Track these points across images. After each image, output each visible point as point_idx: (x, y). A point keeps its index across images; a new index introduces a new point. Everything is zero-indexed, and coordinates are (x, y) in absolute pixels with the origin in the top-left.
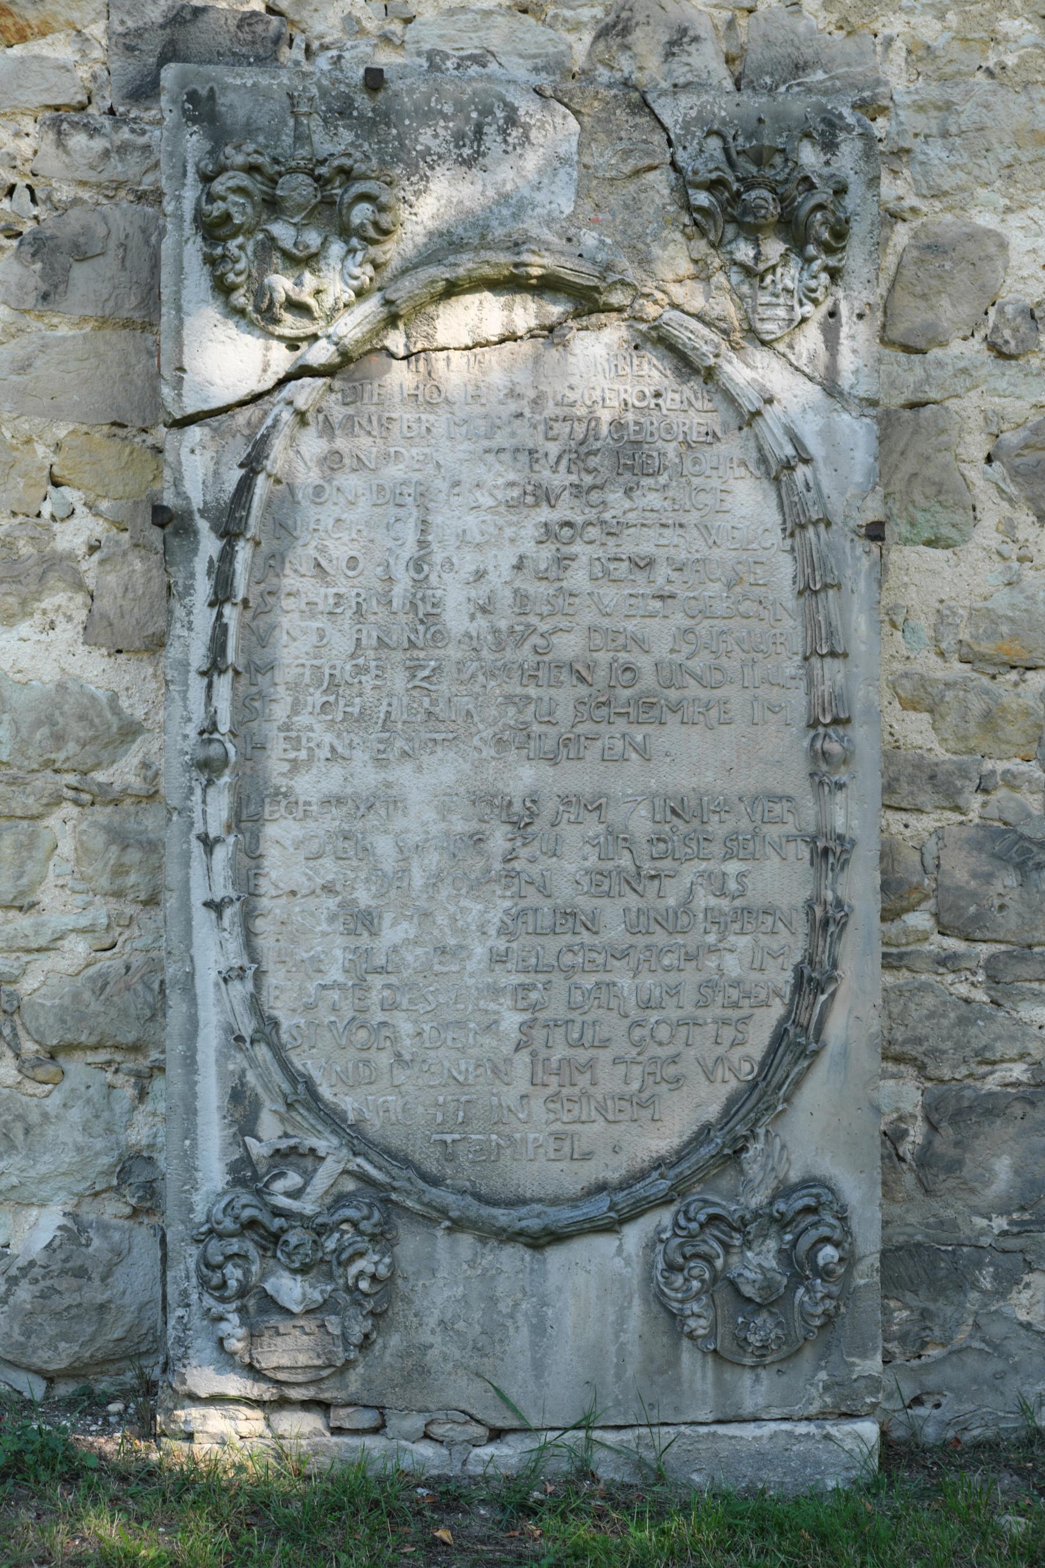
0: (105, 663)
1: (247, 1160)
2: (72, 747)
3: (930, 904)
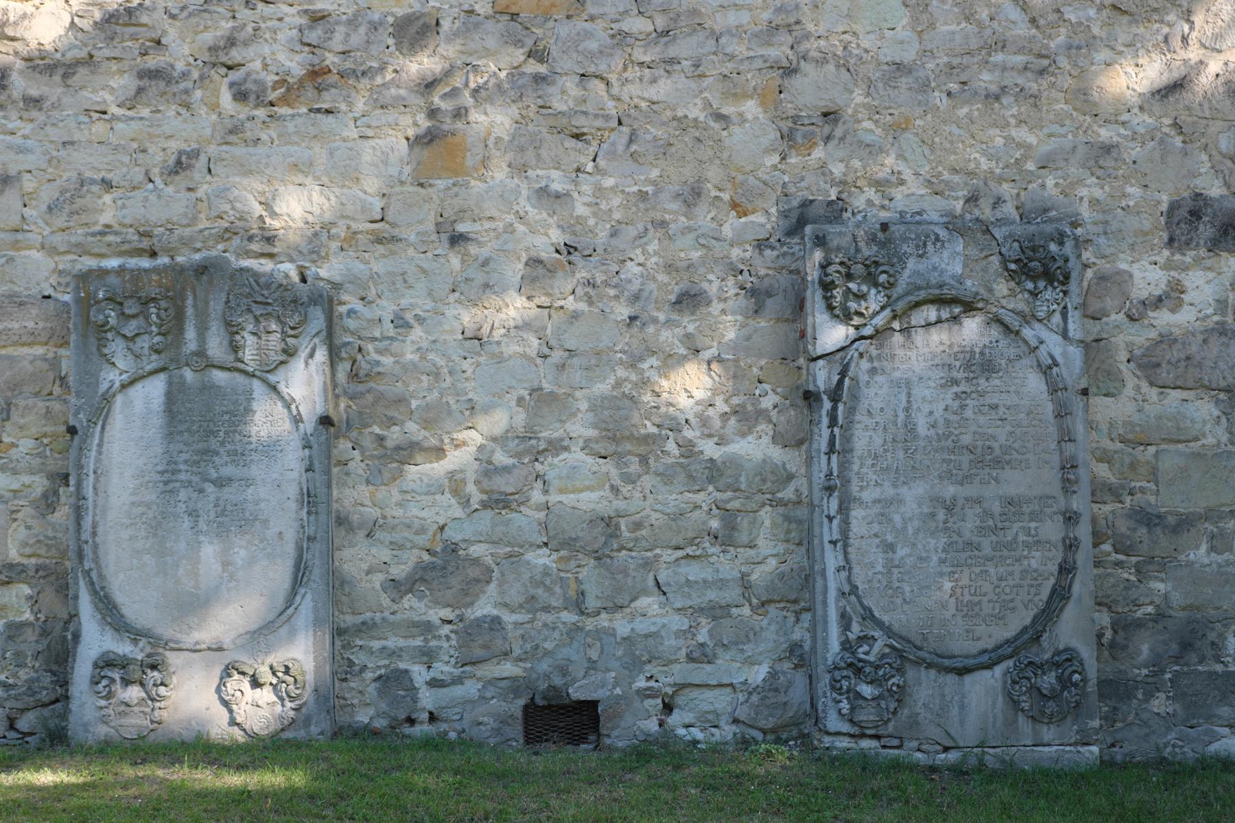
0: (781, 451)
1: (847, 641)
2: (769, 484)
3: (1111, 541)
